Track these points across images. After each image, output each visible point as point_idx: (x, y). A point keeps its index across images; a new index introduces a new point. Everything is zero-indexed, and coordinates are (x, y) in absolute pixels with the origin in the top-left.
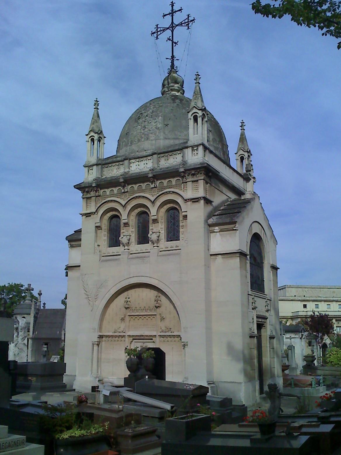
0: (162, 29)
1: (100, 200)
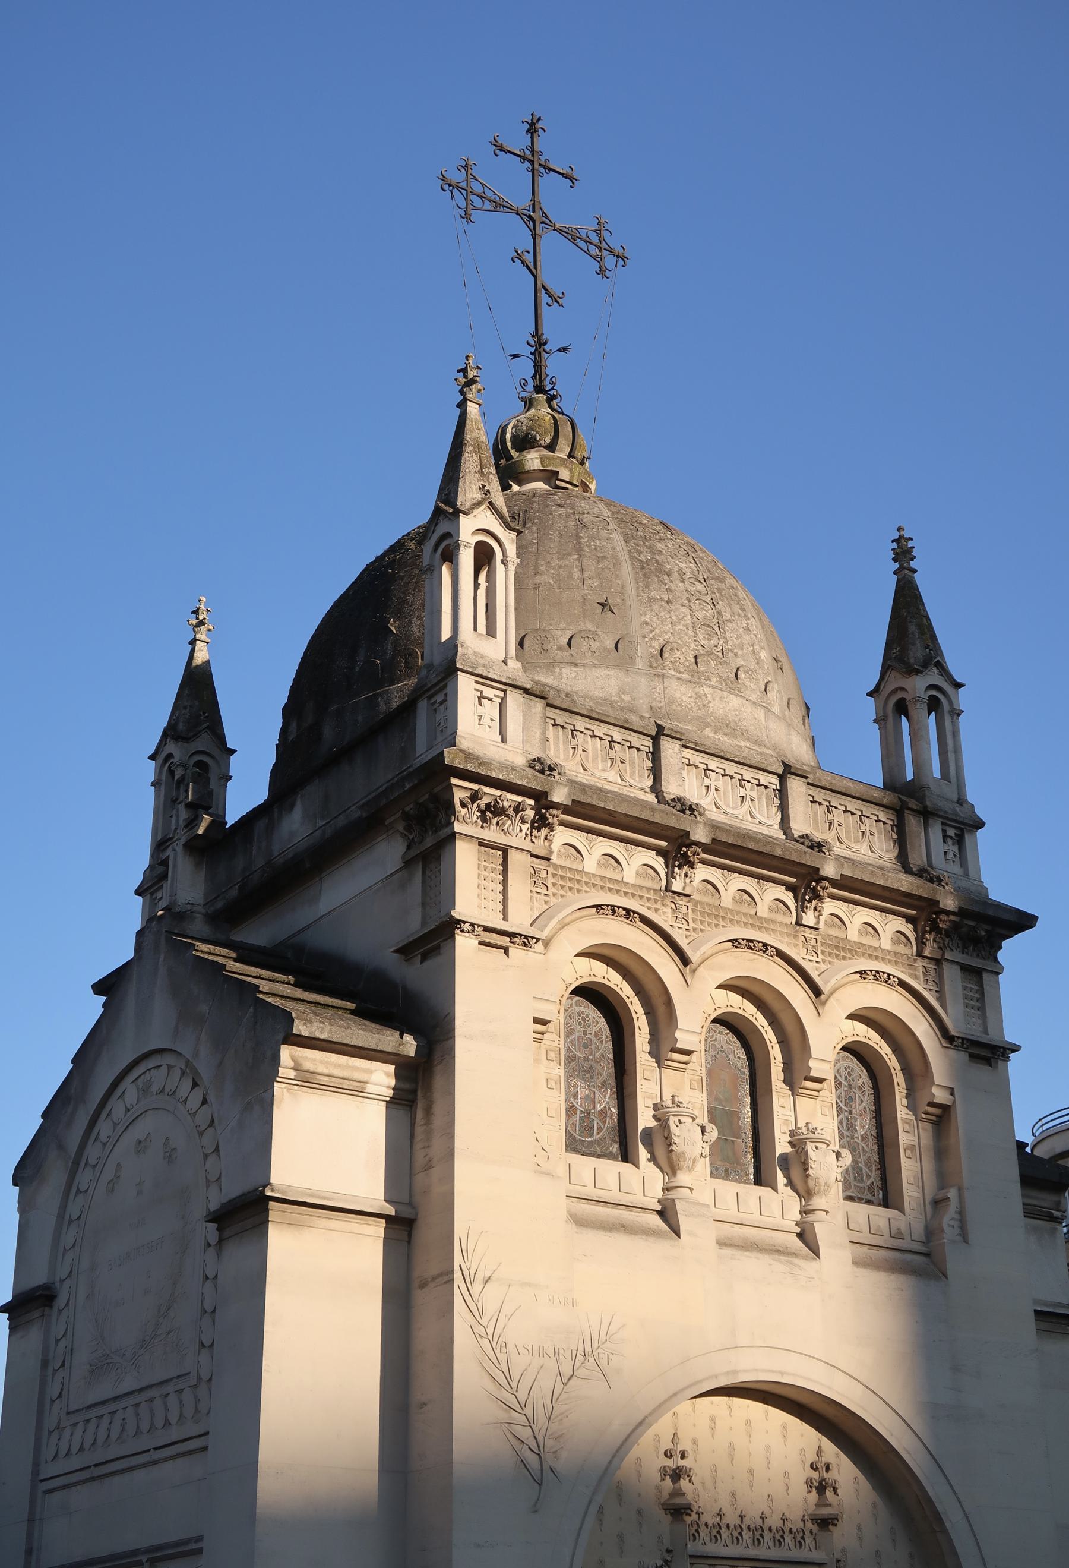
0: (489, 194)
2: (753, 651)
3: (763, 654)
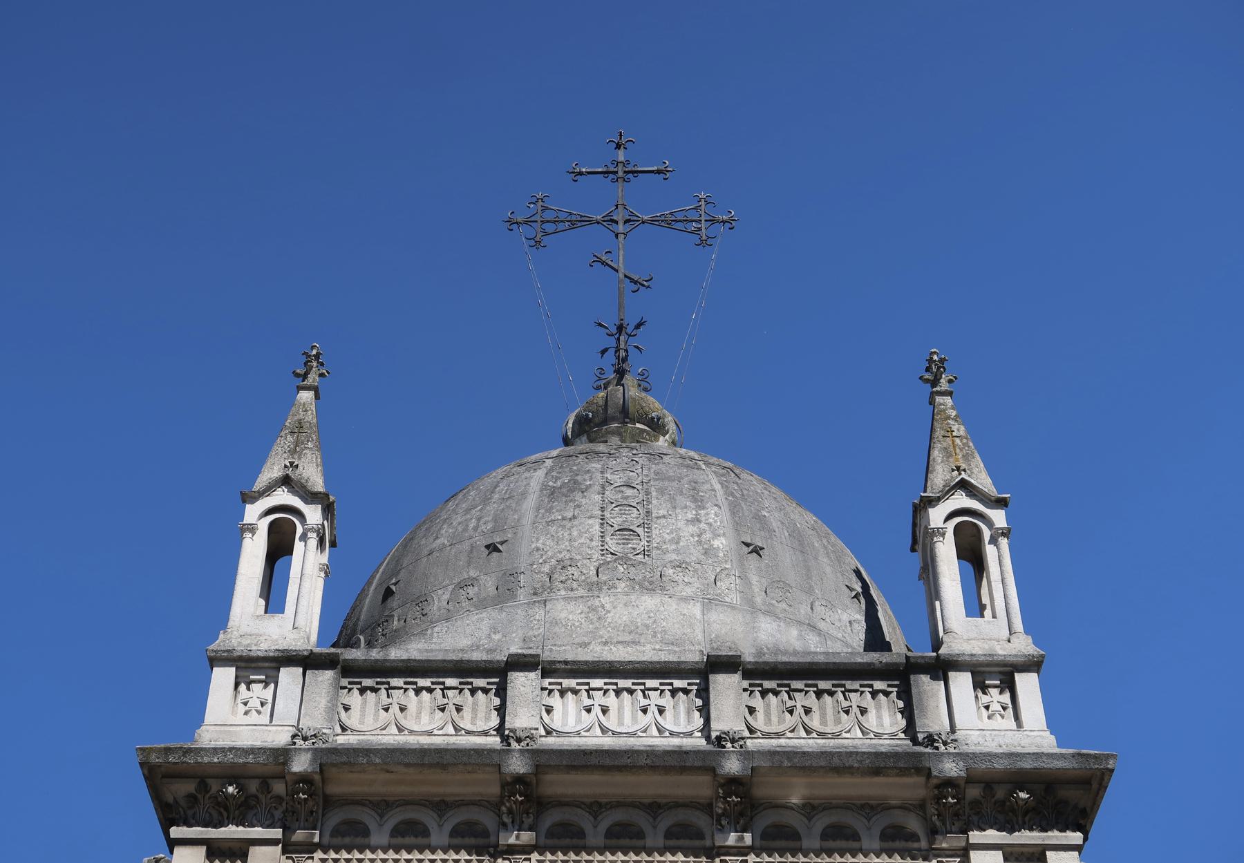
2: (700, 542)
3: (719, 543)
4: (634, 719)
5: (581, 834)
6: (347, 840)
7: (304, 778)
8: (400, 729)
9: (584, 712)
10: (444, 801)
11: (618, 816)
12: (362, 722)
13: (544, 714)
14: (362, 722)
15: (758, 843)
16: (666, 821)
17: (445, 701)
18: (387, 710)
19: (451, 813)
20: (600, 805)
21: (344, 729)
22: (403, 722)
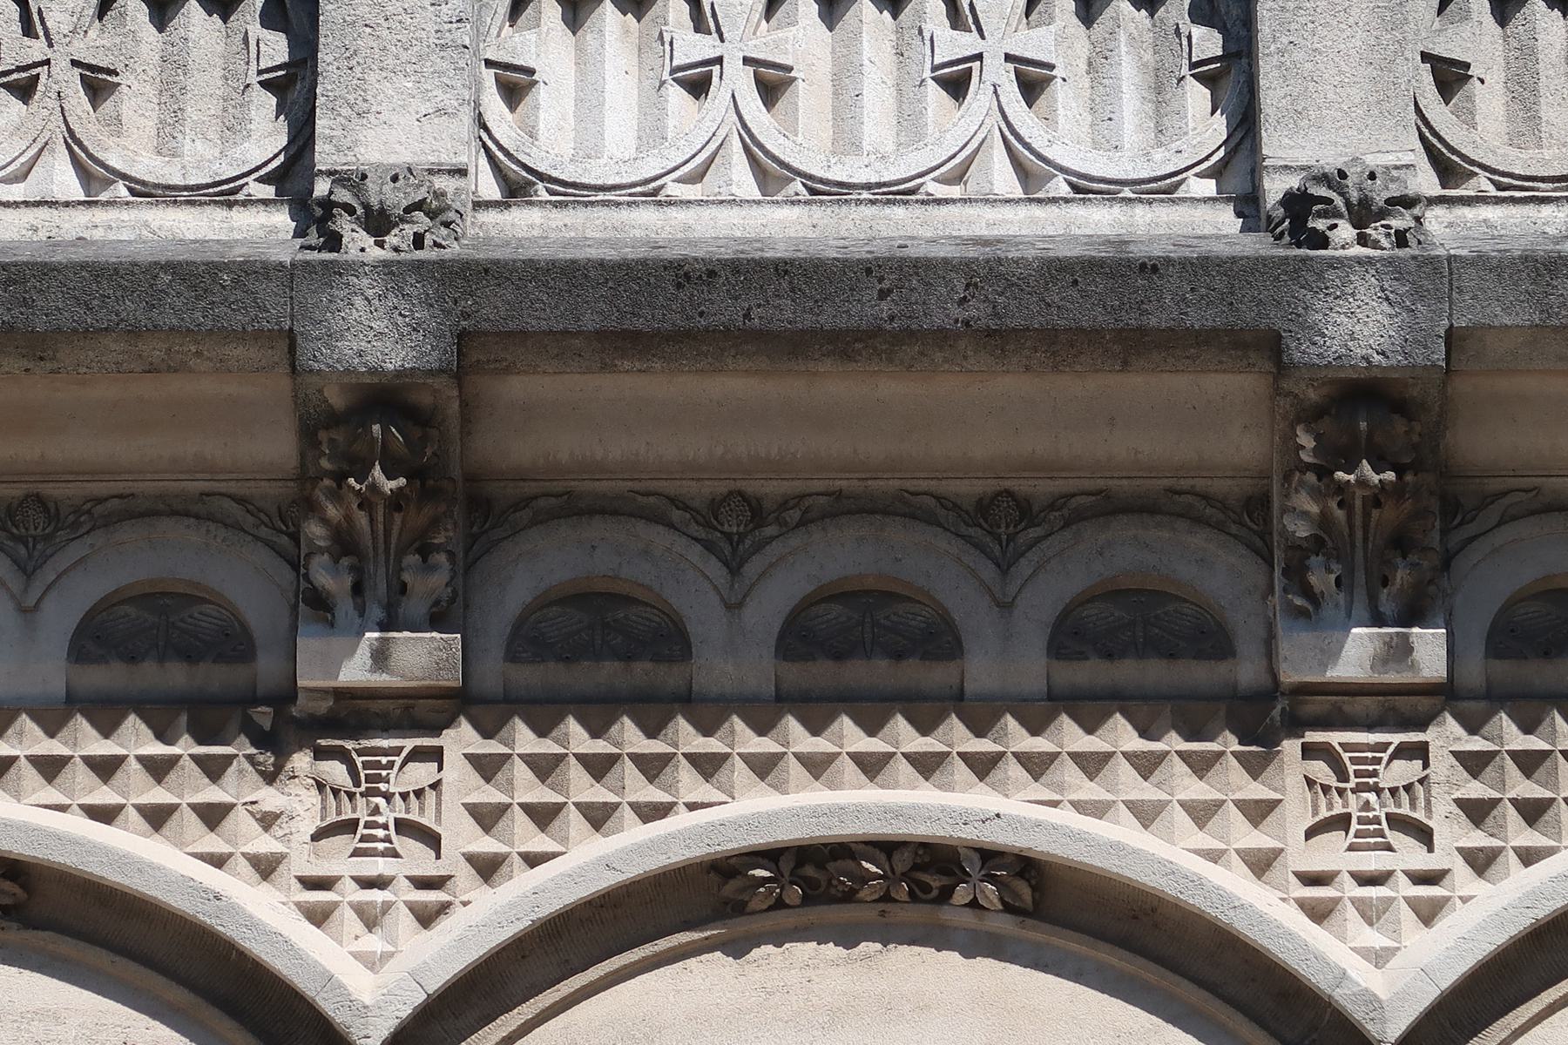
1: (461, 836)
4: (909, 123)
5: (672, 640)
6: (606, 674)
7: (383, 398)
8: (770, 173)
9: (677, 96)
10: (39, 499)
11: (1127, 552)
12: (846, 140)
13: (78, 99)
14: (846, 140)
15: (1475, 672)
16: (1059, 578)
17: (36, 50)
18: (698, 87)
19: (75, 551)
20: (756, 510)
21: (1448, 166)
22: (775, 143)
